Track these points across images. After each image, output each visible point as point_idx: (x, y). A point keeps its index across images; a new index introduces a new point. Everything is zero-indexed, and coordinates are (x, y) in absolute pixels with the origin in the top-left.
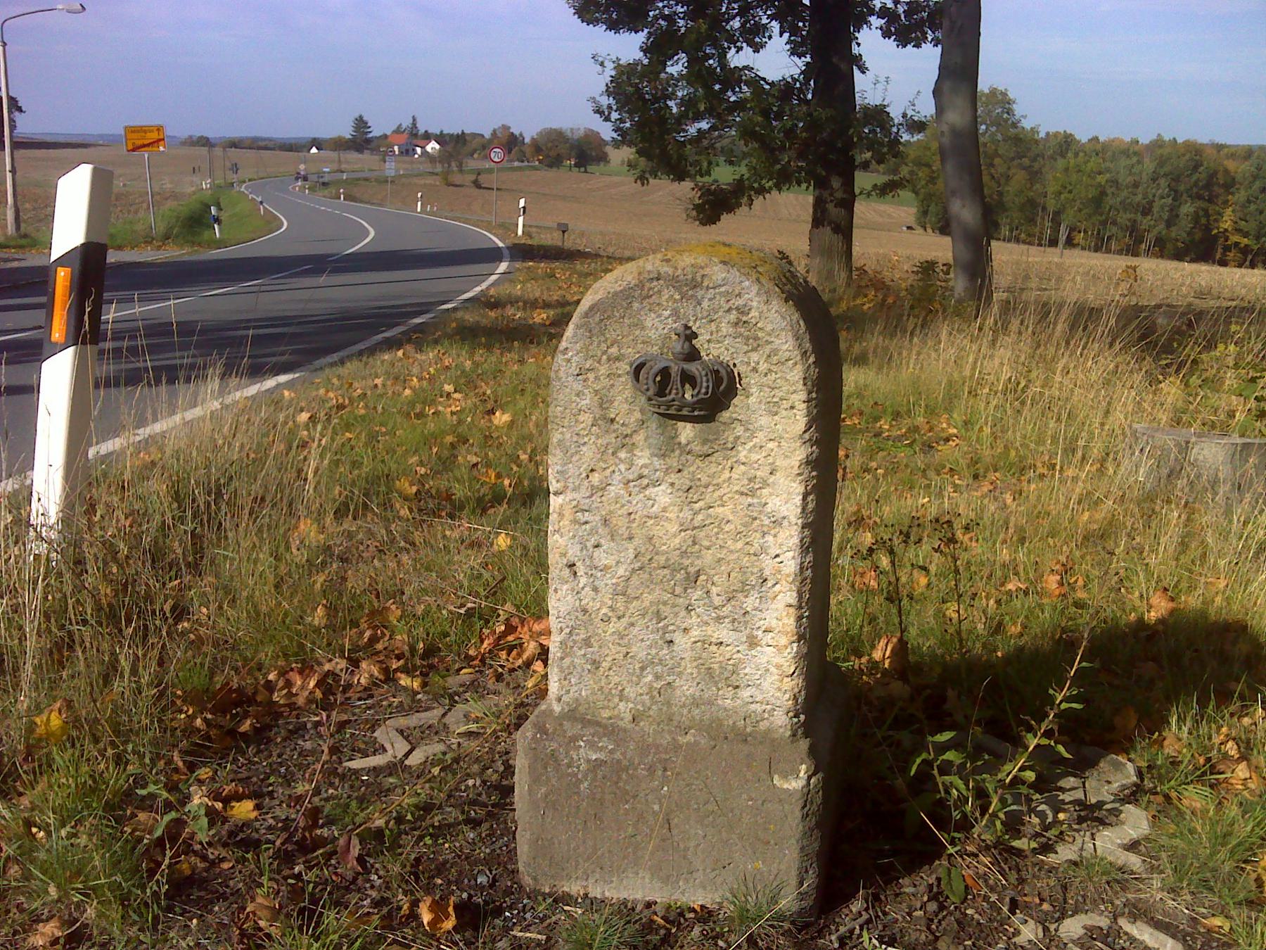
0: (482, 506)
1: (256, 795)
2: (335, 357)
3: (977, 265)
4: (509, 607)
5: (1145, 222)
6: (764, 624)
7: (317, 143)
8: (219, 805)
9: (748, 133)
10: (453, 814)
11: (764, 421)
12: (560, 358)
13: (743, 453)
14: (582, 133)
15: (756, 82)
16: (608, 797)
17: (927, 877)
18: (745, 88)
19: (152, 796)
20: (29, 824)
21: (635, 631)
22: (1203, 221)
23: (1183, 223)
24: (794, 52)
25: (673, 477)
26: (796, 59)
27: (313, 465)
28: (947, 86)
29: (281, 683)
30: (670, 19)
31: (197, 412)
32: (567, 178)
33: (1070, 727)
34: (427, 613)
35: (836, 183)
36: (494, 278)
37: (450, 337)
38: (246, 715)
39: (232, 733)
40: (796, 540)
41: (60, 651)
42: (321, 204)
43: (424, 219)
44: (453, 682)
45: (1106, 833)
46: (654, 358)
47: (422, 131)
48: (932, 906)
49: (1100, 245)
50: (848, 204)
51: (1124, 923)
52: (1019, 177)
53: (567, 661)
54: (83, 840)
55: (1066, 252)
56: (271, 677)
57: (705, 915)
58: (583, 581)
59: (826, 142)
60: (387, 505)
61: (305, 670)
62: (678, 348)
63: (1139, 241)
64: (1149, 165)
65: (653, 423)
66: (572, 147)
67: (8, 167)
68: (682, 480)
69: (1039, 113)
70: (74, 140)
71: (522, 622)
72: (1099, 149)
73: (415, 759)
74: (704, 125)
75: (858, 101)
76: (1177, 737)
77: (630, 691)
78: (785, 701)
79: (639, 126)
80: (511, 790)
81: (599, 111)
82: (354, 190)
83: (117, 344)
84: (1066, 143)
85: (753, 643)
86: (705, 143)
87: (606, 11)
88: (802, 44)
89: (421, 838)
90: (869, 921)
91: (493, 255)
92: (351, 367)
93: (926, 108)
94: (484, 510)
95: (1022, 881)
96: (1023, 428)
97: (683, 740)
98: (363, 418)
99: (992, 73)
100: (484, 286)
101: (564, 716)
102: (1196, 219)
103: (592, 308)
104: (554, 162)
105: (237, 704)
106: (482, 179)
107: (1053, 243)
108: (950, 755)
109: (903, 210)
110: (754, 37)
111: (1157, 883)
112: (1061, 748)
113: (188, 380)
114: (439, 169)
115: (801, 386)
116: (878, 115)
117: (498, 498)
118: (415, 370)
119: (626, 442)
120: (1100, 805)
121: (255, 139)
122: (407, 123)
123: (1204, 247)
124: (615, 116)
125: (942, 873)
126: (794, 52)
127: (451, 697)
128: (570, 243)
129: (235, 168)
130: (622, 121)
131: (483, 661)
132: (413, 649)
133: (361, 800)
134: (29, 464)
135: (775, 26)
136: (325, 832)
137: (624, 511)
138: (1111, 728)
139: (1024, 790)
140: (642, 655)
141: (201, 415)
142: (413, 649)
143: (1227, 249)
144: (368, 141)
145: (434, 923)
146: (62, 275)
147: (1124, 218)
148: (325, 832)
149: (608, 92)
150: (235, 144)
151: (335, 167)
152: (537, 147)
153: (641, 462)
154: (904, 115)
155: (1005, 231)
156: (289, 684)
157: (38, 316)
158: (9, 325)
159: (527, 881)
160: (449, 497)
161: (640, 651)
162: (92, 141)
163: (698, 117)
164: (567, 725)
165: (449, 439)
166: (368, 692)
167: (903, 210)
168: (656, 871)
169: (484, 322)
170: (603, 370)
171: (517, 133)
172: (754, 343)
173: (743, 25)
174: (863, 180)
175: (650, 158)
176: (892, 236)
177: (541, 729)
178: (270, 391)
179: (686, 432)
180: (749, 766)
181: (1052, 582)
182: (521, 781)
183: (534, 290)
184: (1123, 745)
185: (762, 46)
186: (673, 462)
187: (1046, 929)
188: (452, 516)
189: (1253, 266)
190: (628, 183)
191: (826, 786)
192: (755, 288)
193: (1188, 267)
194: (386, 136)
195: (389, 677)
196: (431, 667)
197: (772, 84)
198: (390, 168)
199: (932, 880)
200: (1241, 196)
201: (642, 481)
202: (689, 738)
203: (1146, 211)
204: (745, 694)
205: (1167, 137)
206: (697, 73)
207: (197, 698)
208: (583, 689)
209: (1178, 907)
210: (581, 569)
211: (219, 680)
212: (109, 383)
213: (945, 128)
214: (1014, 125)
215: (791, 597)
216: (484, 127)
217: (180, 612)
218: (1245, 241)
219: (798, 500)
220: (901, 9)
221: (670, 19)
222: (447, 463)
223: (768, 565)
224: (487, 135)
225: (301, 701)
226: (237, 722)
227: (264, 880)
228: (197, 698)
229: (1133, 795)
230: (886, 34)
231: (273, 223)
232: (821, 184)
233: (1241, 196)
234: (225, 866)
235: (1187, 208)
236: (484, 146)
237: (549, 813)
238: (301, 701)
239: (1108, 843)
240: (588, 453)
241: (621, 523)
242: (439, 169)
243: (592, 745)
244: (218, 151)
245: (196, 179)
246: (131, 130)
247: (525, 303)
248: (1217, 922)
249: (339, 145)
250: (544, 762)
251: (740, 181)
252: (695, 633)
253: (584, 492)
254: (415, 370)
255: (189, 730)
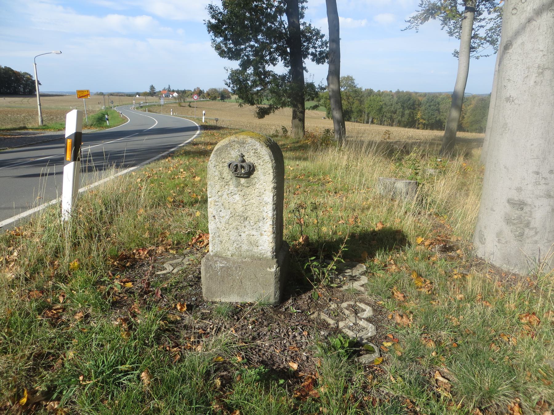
0: (192, 204)
1: (132, 281)
2: (147, 162)
3: (341, 130)
4: (200, 231)
5: (395, 116)
6: (264, 230)
7: (138, 94)
8: (122, 284)
9: (272, 91)
10: (185, 284)
11: (262, 177)
12: (209, 162)
13: (257, 186)
14: (222, 89)
15: (274, 76)
16: (225, 276)
17: (309, 294)
18: (271, 77)
19: (105, 281)
20: (71, 290)
21: (231, 233)
22: (412, 115)
23: (406, 116)
24: (285, 66)
25: (240, 193)
26: (286, 68)
27: (143, 194)
28: (330, 78)
29: (137, 253)
30: (248, 56)
31: (108, 179)
32: (218, 103)
33: (345, 256)
34: (177, 233)
35: (299, 106)
36: (195, 136)
37: (182, 155)
38: (128, 261)
39: (124, 266)
40: (272, 208)
41: (76, 245)
42: (141, 113)
43: (172, 118)
44: (185, 252)
45: (356, 283)
46: (234, 162)
47: (172, 89)
48: (309, 301)
49: (381, 123)
50: (303, 113)
51: (358, 304)
52: (356, 103)
53: (214, 241)
54: (87, 292)
55: (371, 125)
56: (134, 251)
57: (251, 304)
58: (217, 220)
59: (297, 94)
60: (165, 204)
61: (144, 249)
62: (240, 159)
63: (393, 122)
64: (395, 99)
65: (234, 179)
66: (219, 94)
67: (38, 103)
68: (242, 193)
69: (363, 83)
70: (58, 94)
71: (203, 235)
72: (380, 94)
73: (175, 271)
74: (259, 88)
75: (305, 81)
76: (378, 259)
77: (231, 249)
78: (270, 249)
79: (239, 89)
80: (200, 277)
81: (226, 84)
82: (150, 108)
83: (85, 159)
84: (370, 92)
85: (261, 235)
86: (259, 94)
87: (228, 54)
88: (288, 63)
89: (177, 290)
90: (293, 305)
91: (195, 129)
92: (153, 164)
93: (325, 83)
94: (193, 205)
95: (333, 294)
96: (348, 180)
97: (244, 260)
98: (157, 180)
99: (344, 73)
100: (192, 138)
101: (213, 256)
102: (410, 115)
103: (217, 149)
104: (214, 98)
105: (125, 259)
106: (191, 104)
107: (367, 122)
108: (315, 263)
109: (322, 113)
110: (273, 61)
111: (366, 294)
112: (342, 260)
113: (105, 169)
114: (177, 101)
115: (271, 168)
116: (311, 85)
117: (196, 202)
118: (172, 165)
119: (227, 184)
120: (355, 276)
121: (119, 93)
122: (167, 87)
123: (412, 123)
124: (231, 85)
125: (312, 293)
126: (285, 66)
127: (184, 255)
128: (219, 124)
129: (112, 102)
130: (234, 87)
131: (193, 246)
132: (173, 243)
133: (161, 281)
134: (61, 194)
135: (280, 58)
136: (151, 289)
137: (227, 202)
138: (361, 257)
139: (333, 271)
140: (233, 239)
141: (109, 180)
142: (173, 243)
143: (419, 124)
144: (155, 93)
145: (181, 309)
146: (69, 142)
147: (388, 115)
148: (151, 289)
149: (229, 78)
150: (112, 94)
151: (145, 101)
152: (208, 94)
153: (231, 189)
154: (319, 85)
155: (353, 119)
156: (139, 253)
157: (62, 151)
158: (43, 154)
159: (205, 299)
160: (182, 202)
161: (233, 238)
162: (64, 94)
163: (257, 86)
164: (214, 258)
165: (182, 185)
166: (161, 255)
167: (322, 113)
168: (238, 294)
169: (192, 150)
170: (221, 165)
171: (202, 90)
172: (259, 158)
173: (270, 58)
174: (308, 104)
175: (243, 99)
176: (318, 121)
177: (208, 259)
178: (129, 172)
179: (243, 181)
180: (261, 266)
181: (351, 220)
182: (203, 275)
183: (208, 139)
184: (363, 261)
185: (276, 64)
186: (239, 189)
187: (338, 305)
188: (183, 207)
189: (427, 129)
190: (236, 105)
191: (281, 270)
192: (259, 144)
193: (407, 129)
194: (160, 91)
195: (167, 251)
196: (179, 248)
197: (280, 76)
198: (162, 102)
199: (310, 295)
200: (423, 108)
201: (232, 194)
202: (246, 260)
203: (395, 113)
204: (260, 248)
205: (401, 90)
206: (257, 73)
207: (115, 257)
208: (218, 248)
209: (371, 299)
210: (216, 217)
211: (120, 253)
212: (83, 170)
213: (330, 90)
214: (355, 87)
215: (271, 223)
216: (191, 88)
217: (108, 235)
218: (424, 122)
219: (272, 198)
220: (317, 53)
221: (248, 56)
222: (182, 192)
223: (265, 215)
224: (193, 90)
225: (143, 258)
226: (126, 263)
227: (136, 300)
228: (115, 257)
229: (364, 274)
230: (313, 60)
231: (124, 120)
232: (294, 106)
233: (423, 108)
234: (125, 298)
235: (407, 112)
236: (192, 94)
237: (210, 281)
238: (143, 258)
239: (356, 285)
240: (218, 187)
241: (227, 205)
242: (177, 101)
243: (221, 262)
244: (106, 97)
245: (100, 106)
246: (79, 92)
247: (205, 144)
248: (381, 302)
249: (145, 94)
250: (208, 267)
251: (270, 105)
252: (247, 233)
253: (217, 197)
254: (172, 165)
255: (113, 265)
